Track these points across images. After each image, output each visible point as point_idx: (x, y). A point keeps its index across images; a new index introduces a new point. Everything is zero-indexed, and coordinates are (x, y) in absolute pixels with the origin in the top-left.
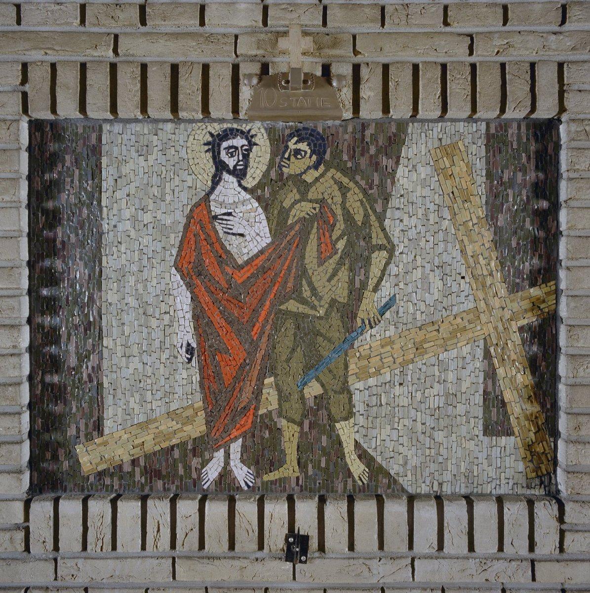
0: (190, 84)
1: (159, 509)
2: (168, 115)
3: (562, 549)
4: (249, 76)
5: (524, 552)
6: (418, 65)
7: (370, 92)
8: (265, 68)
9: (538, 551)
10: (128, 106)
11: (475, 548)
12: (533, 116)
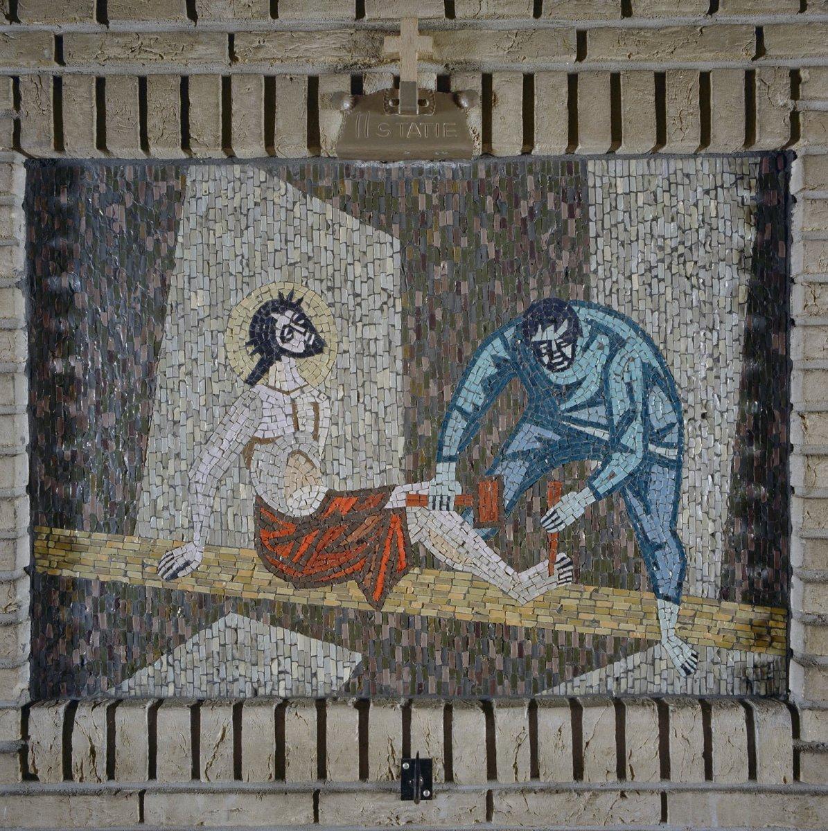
0: (682, 103)
1: (512, 721)
2: (219, 154)
4: (339, 97)
7: (80, 111)
8: (357, 85)
10: (639, 138)
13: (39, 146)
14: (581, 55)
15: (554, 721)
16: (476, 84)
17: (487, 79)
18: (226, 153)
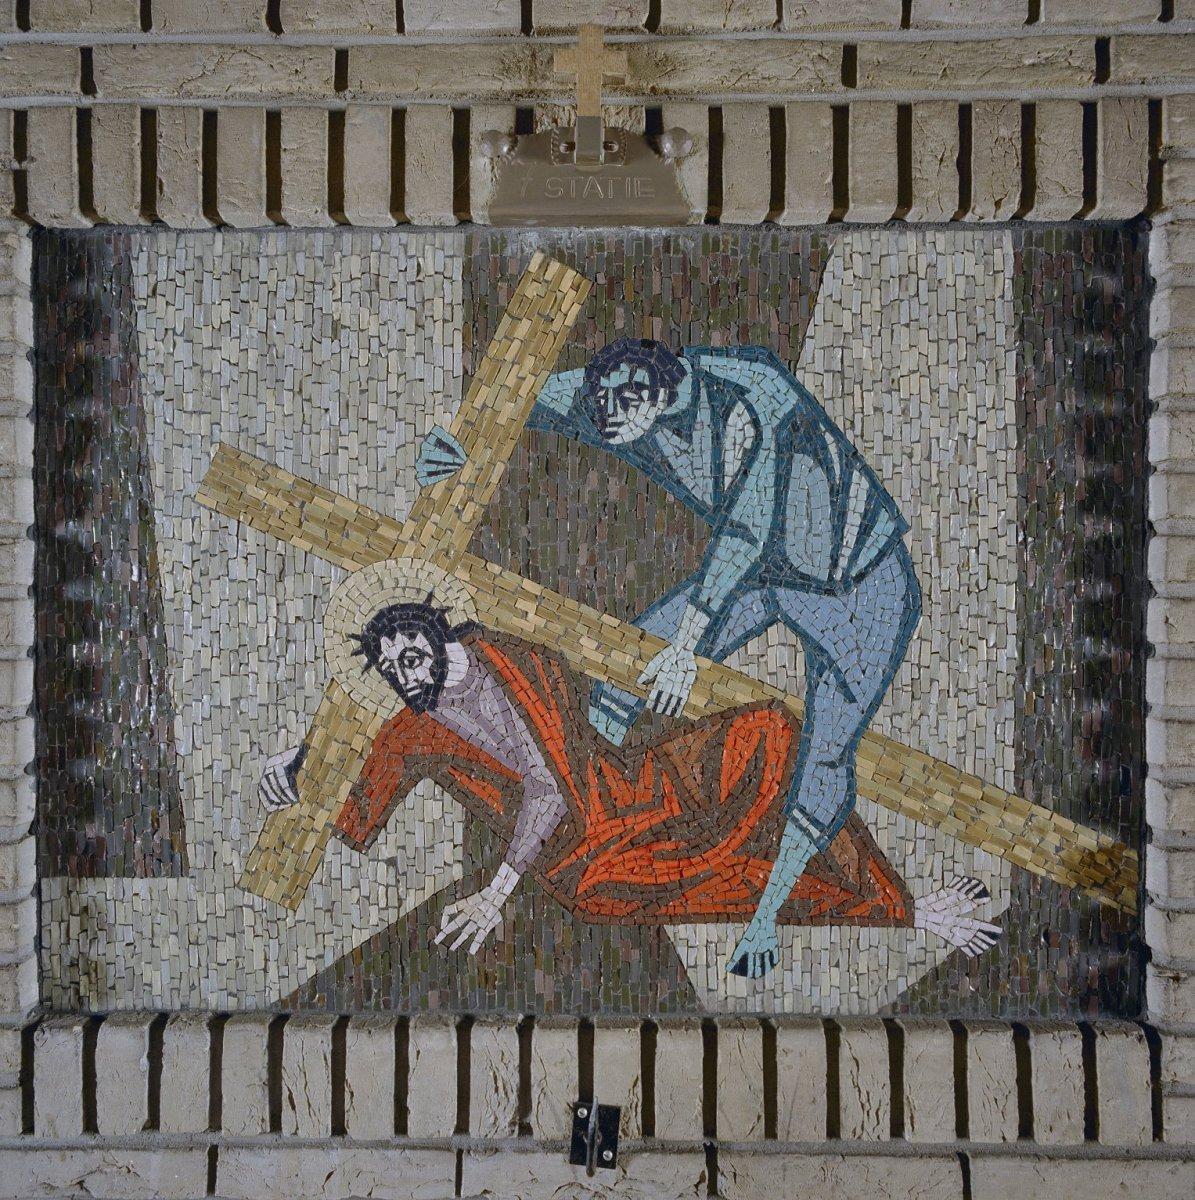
1: (494, 1045)
4: (493, 136)
5: (947, 1136)
8: (524, 121)
13: (55, 205)
14: (1102, 75)
16: (700, 126)
17: (715, 114)
18: (211, 219)
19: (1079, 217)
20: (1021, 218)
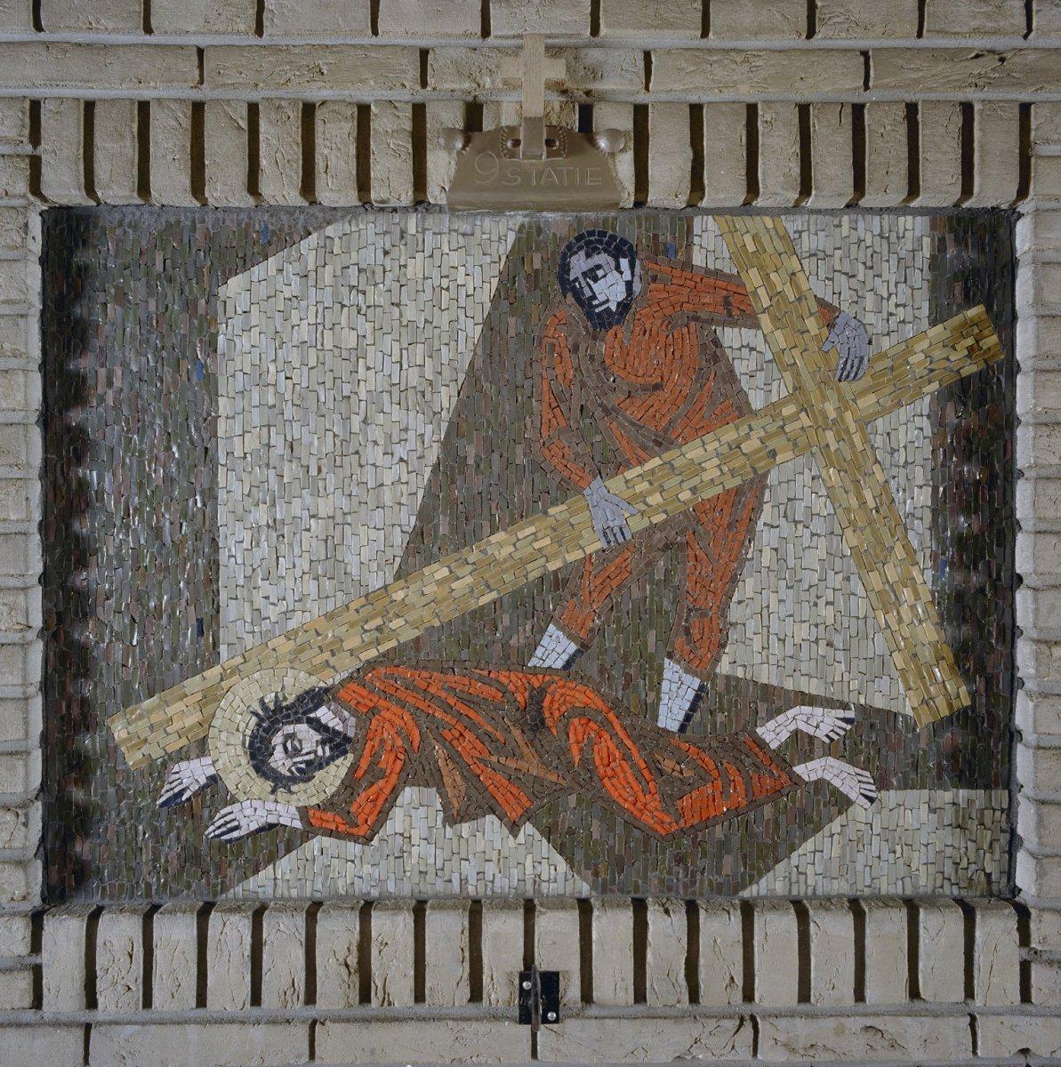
0: (723, 140)
1: (119, 931)
3: (914, 993)
4: (450, 132)
6: (368, 107)
7: (115, 153)
9: (978, 1001)
11: (208, 1003)
12: (966, 205)
13: (63, 187)
15: (230, 932)
16: (626, 123)
19: (957, 205)
20: (750, 204)
